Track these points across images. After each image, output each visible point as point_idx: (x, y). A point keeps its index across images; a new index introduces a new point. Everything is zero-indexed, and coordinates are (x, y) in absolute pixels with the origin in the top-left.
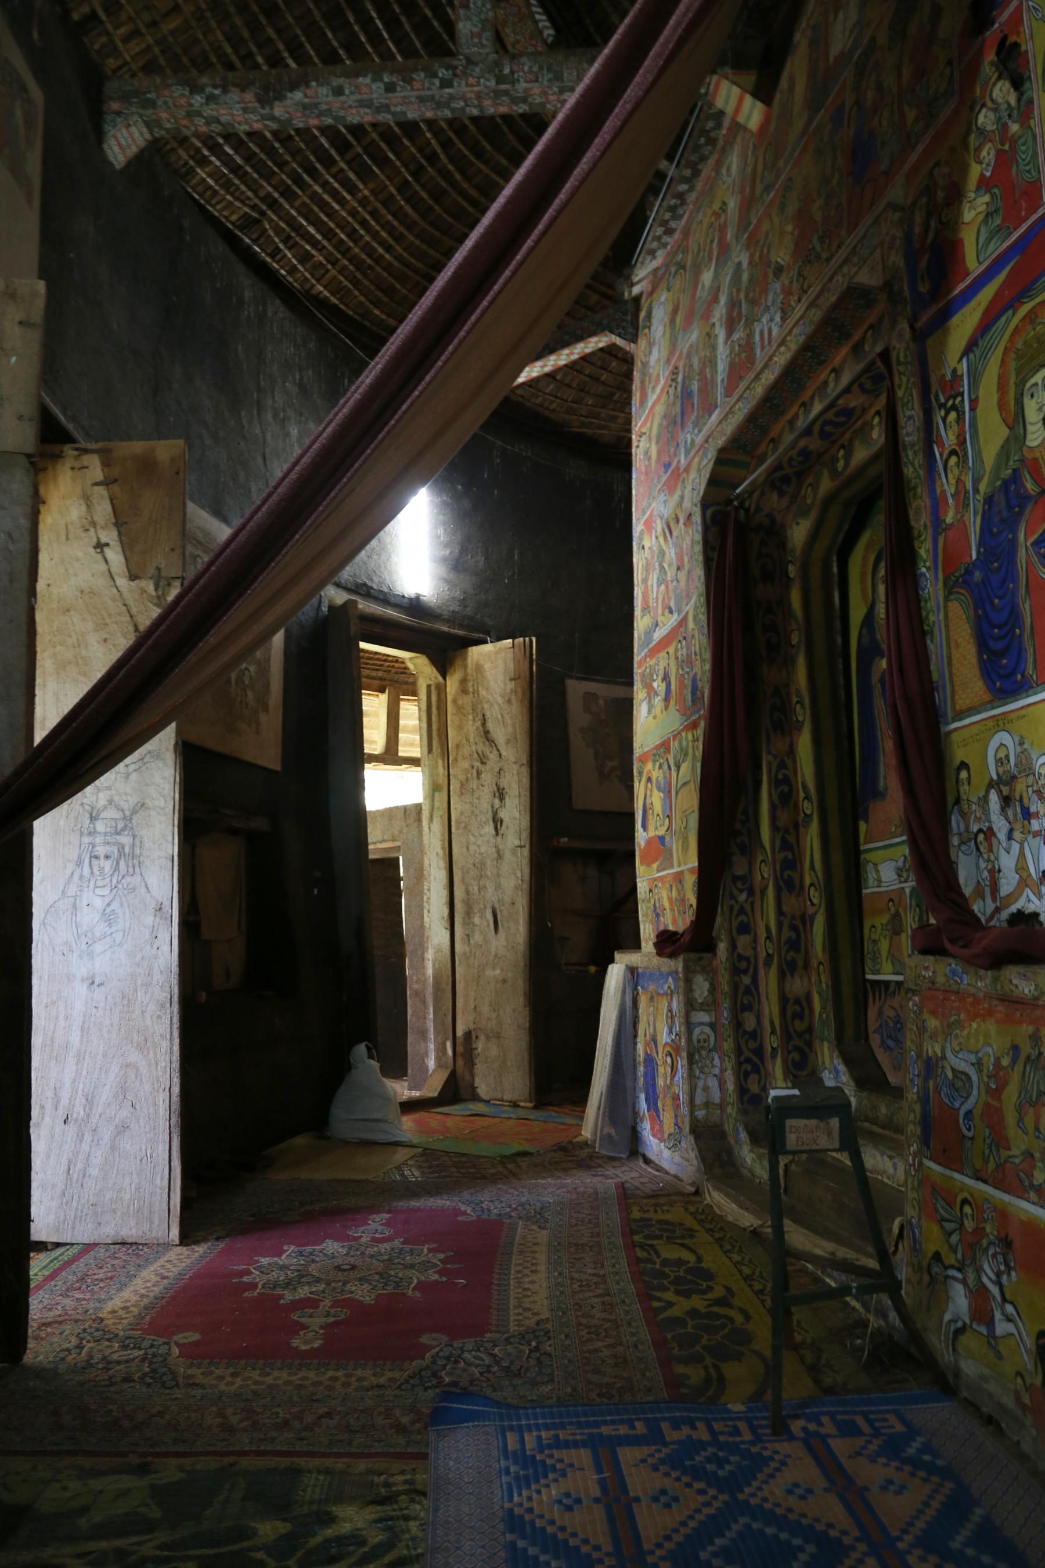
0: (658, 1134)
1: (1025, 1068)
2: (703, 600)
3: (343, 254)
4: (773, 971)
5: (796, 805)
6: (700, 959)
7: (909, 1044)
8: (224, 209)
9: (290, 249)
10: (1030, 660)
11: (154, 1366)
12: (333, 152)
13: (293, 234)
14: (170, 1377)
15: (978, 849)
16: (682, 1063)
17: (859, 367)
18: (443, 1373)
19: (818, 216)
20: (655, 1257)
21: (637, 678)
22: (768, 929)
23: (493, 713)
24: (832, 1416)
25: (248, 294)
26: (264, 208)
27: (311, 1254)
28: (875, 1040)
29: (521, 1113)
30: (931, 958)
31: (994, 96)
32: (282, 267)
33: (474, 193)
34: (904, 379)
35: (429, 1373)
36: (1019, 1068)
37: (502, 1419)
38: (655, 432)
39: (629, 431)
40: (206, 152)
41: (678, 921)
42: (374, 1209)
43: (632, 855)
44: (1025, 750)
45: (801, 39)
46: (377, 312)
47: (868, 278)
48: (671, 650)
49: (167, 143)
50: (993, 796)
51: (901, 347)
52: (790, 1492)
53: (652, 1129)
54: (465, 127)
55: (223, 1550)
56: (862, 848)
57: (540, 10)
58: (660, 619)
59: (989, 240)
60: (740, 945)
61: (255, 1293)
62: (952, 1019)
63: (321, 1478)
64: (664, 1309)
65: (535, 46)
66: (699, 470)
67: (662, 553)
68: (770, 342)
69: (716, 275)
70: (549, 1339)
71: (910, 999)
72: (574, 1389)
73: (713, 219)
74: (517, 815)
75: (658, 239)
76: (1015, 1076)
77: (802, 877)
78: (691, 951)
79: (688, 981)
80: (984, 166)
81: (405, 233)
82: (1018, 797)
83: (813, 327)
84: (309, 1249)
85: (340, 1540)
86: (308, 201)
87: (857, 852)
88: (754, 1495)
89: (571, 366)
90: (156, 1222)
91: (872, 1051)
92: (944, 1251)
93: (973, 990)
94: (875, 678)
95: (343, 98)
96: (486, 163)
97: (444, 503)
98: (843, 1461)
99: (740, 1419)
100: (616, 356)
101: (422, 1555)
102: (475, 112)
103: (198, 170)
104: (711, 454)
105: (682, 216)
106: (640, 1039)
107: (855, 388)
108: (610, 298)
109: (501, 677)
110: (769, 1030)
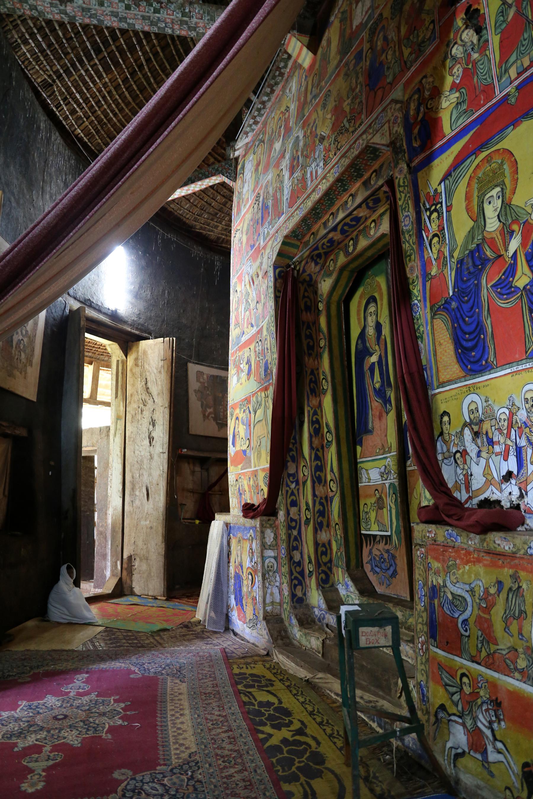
0: (243, 619)
1: (508, 595)
2: (273, 319)
3: (92, 113)
4: (310, 528)
5: (323, 435)
6: (269, 520)
8: (35, 73)
9: (66, 105)
12: (92, 52)
13: (68, 97)
15: (456, 462)
16: (258, 579)
19: (347, 109)
20: (253, 701)
22: (307, 504)
23: (151, 378)
25: (42, 125)
28: (367, 568)
29: (159, 603)
30: (434, 526)
31: (463, 38)
36: (503, 595)
38: (245, 228)
42: (77, 671)
48: (252, 347)
50: (467, 432)
53: (239, 616)
56: (358, 460)
58: (245, 330)
59: (458, 118)
60: (291, 513)
62: (450, 563)
66: (272, 248)
67: (248, 294)
68: (316, 178)
69: (283, 144)
71: (419, 549)
73: (281, 116)
74: (162, 435)
75: (250, 126)
78: (265, 515)
79: (262, 532)
80: (455, 77)
81: (124, 107)
82: (484, 433)
83: (344, 168)
86: (78, 79)
87: (356, 463)
89: (204, 191)
91: (366, 574)
92: (448, 704)
93: (465, 546)
100: (220, 193)
103: (22, 46)
104: (280, 239)
105: (263, 115)
106: (232, 564)
107: (364, 205)
109: (156, 359)
110: (308, 561)
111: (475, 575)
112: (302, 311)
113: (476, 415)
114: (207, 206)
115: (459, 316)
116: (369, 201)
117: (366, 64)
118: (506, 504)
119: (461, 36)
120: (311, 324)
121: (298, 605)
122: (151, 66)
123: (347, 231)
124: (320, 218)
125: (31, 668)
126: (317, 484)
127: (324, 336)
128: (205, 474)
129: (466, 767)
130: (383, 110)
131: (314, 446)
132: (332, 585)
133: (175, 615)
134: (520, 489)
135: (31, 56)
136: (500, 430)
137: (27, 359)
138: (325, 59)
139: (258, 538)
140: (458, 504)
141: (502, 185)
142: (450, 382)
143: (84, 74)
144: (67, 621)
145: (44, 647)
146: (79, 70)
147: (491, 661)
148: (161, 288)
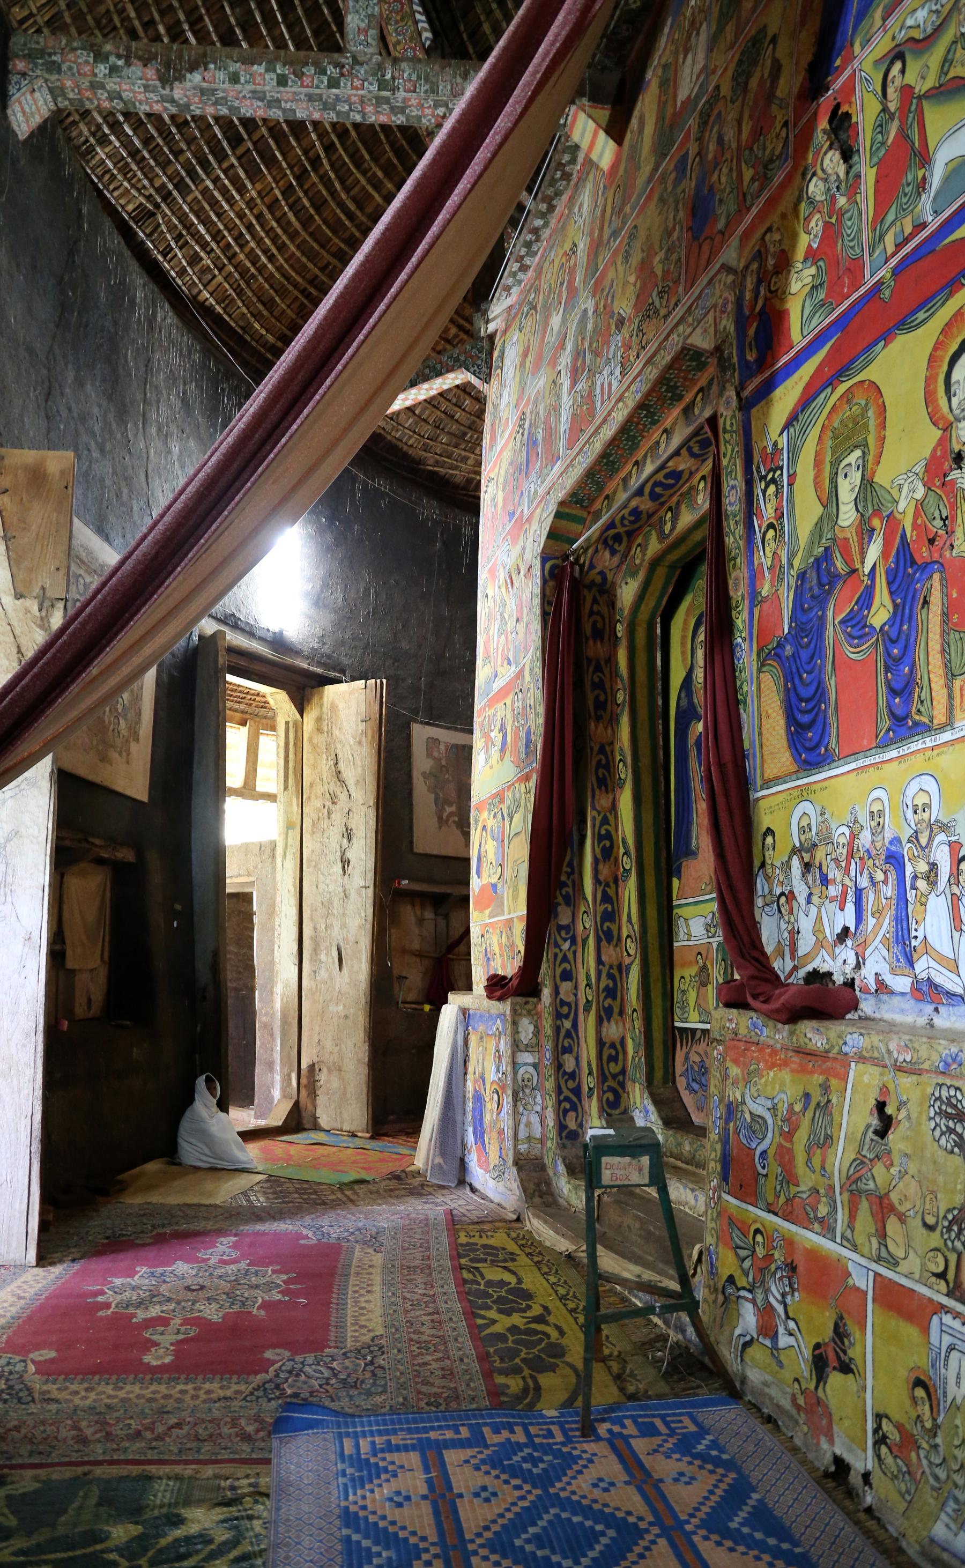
0: (484, 1165)
2: (539, 653)
3: (230, 259)
5: (616, 859)
6: (526, 1003)
7: (712, 1089)
8: (121, 196)
9: (181, 248)
10: (834, 734)
11: (10, 1383)
12: (225, 144)
13: (184, 232)
14: (26, 1393)
16: (507, 1100)
17: (689, 430)
18: (285, 1386)
19: (659, 270)
20: (479, 1279)
21: (476, 727)
22: (588, 976)
24: (634, 1419)
25: (139, 295)
26: (159, 200)
27: (162, 1275)
28: (681, 1083)
29: (358, 1142)
30: (735, 1011)
32: (172, 268)
33: (352, 206)
34: (729, 448)
35: (273, 1386)
36: (809, 1114)
37: (339, 1427)
39: (479, 474)
40: (107, 130)
41: (509, 967)
42: (221, 1232)
43: (466, 899)
44: (826, 820)
45: (652, 76)
46: (257, 326)
47: (702, 341)
48: (508, 701)
49: (69, 115)
51: (729, 416)
52: (595, 1486)
53: (479, 1160)
54: (347, 130)
55: (78, 1553)
56: (675, 903)
57: (420, 9)
58: (500, 669)
61: (109, 1312)
63: (171, 1483)
64: (487, 1326)
65: (415, 50)
66: (540, 522)
69: (564, 321)
70: (383, 1353)
72: (405, 1399)
73: (564, 260)
74: (363, 856)
75: (514, 274)
76: (806, 1121)
77: (620, 928)
78: (519, 995)
79: (515, 1023)
81: (288, 242)
84: (160, 1270)
85: (188, 1540)
86: (200, 197)
87: (670, 908)
88: (563, 1489)
89: (429, 401)
90: (14, 1244)
92: (738, 1275)
93: (771, 1042)
94: (691, 741)
95: (238, 87)
96: (364, 173)
97: (310, 536)
98: (642, 1457)
99: (553, 1423)
100: (469, 394)
101: (265, 1550)
102: (358, 118)
103: (98, 149)
104: (552, 507)
105: (536, 253)
106: (470, 1076)
107: (684, 452)
108: (467, 332)
111: (780, 1085)
112: (587, 639)
113: (808, 836)
114: (446, 420)
115: (794, 670)
116: (691, 443)
117: (689, 184)
118: (839, 979)
119: (822, 164)
120: (602, 663)
121: (568, 1143)
122: (334, 158)
123: (662, 496)
124: (618, 470)
125: (154, 1227)
126: (604, 943)
127: (623, 684)
128: (442, 923)
129: (753, 1359)
130: (710, 282)
131: (602, 878)
132: (625, 1111)
133: (382, 1160)
134: (857, 955)
135: (115, 165)
136: (836, 860)
137: (130, 729)
138: (634, 157)
139: (508, 1032)
140: (773, 979)
141: (864, 445)
142: (778, 780)
143: (211, 187)
144: (208, 1165)
145: (174, 1199)
146: (203, 180)
147: (789, 1209)
148: (362, 586)
